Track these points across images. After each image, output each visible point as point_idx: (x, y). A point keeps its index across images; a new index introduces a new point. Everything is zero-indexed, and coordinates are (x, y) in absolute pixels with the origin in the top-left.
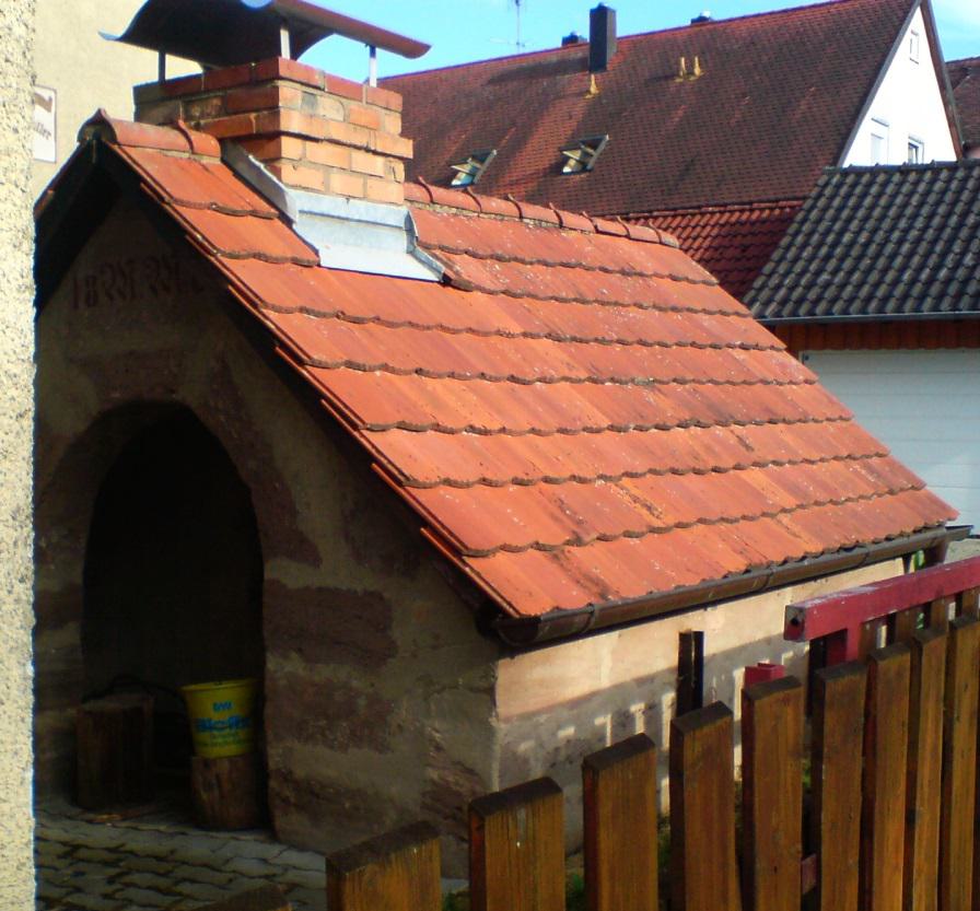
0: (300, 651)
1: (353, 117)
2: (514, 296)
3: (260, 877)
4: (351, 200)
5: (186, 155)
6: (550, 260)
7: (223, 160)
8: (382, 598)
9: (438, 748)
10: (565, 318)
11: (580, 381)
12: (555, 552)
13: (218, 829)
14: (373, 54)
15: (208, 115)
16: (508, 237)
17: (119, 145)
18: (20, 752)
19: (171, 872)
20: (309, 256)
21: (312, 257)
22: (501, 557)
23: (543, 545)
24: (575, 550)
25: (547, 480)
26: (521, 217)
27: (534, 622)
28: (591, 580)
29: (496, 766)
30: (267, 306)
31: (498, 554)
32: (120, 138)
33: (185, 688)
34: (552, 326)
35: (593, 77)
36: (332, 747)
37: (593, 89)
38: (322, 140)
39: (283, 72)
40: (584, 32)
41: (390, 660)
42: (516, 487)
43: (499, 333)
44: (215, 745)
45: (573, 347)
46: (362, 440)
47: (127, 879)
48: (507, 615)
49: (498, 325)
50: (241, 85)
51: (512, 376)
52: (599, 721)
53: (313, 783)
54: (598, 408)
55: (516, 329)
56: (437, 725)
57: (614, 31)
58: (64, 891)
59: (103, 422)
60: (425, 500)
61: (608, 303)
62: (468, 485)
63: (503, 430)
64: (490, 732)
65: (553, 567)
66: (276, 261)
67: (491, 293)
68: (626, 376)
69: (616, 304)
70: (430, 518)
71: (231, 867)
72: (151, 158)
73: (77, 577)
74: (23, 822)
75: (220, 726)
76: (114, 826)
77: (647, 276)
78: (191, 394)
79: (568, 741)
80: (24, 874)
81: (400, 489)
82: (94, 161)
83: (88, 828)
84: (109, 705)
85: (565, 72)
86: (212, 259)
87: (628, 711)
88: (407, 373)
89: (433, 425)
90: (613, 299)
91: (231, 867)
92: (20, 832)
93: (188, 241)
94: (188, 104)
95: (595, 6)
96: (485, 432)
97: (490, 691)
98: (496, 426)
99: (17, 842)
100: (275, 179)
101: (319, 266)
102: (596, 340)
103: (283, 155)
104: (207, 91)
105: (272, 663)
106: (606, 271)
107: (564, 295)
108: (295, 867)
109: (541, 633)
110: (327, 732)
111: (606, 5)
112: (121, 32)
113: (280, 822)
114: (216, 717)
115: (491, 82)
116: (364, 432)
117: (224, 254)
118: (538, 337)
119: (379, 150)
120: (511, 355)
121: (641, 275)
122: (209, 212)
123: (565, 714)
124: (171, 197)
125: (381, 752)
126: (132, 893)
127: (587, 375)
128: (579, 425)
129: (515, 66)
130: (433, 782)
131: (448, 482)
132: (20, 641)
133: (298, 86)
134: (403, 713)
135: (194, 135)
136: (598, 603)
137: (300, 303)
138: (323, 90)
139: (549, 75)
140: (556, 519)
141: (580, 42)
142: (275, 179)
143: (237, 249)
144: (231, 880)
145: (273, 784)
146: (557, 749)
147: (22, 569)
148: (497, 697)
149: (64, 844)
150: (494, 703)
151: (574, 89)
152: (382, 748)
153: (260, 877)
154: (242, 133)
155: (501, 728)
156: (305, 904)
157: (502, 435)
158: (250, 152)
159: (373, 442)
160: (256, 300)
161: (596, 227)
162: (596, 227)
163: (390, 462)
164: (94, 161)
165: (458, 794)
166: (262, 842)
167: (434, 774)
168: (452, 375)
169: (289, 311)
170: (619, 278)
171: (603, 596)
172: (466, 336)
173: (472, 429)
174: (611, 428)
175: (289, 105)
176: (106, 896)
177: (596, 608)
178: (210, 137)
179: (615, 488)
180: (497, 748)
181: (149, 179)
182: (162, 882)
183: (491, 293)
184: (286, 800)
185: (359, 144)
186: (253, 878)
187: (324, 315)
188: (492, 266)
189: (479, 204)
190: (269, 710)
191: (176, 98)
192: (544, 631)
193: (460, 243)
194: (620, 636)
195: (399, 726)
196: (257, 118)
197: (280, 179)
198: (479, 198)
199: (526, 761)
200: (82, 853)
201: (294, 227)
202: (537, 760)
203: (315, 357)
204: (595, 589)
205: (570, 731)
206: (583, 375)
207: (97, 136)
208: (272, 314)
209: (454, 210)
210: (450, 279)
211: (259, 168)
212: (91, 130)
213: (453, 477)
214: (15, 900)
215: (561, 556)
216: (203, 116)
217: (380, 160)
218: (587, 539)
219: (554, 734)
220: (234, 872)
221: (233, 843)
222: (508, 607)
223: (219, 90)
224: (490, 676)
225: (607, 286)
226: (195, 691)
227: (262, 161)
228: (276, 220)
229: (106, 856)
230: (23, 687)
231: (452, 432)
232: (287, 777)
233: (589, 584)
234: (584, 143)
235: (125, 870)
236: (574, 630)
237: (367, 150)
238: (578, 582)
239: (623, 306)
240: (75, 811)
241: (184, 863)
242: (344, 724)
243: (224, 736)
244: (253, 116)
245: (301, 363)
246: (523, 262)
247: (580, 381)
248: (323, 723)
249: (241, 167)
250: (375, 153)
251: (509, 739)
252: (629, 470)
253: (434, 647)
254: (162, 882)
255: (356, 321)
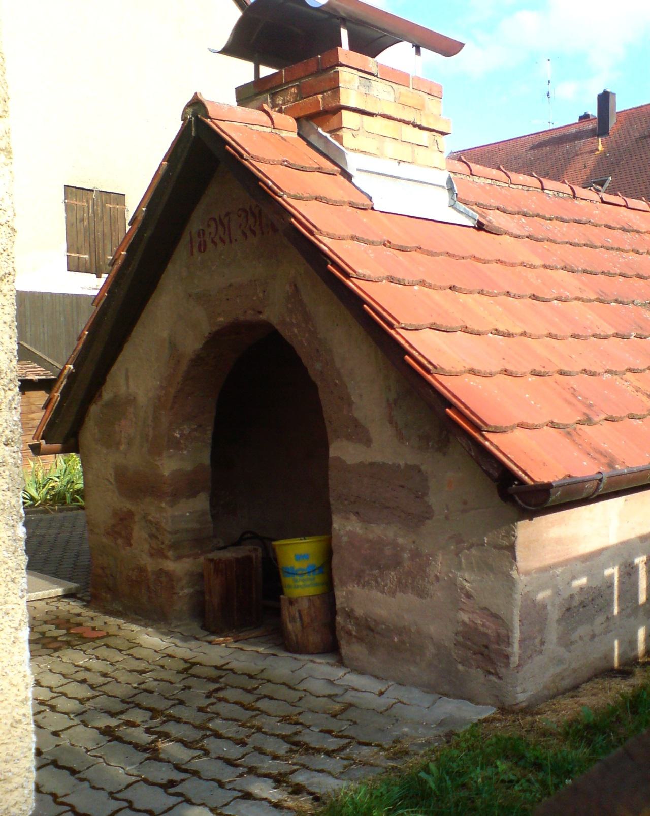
0: (357, 514)
1: (403, 99)
2: (537, 240)
3: (324, 696)
4: (402, 163)
5: (269, 130)
6: (565, 217)
7: (299, 134)
8: (420, 471)
9: (468, 596)
10: (580, 258)
11: (589, 301)
12: (568, 430)
13: (300, 653)
14: (418, 52)
15: (288, 101)
16: (532, 202)
17: (211, 119)
18: (12, 612)
19: (256, 689)
20: (362, 201)
21: (367, 202)
22: (518, 433)
23: (557, 424)
24: (586, 428)
25: (561, 373)
26: (543, 189)
27: (546, 489)
28: (601, 453)
29: (517, 612)
30: (321, 234)
31: (515, 430)
32: (211, 114)
33: (275, 543)
34: (567, 262)
35: (600, 139)
36: (383, 592)
37: (600, 148)
38: (377, 115)
39: (342, 59)
40: (594, 112)
41: (427, 521)
42: (534, 378)
43: (523, 264)
44: (297, 587)
45: (585, 277)
46: (397, 337)
47: (221, 694)
48: (522, 482)
49: (521, 258)
50: (311, 74)
51: (534, 295)
52: (607, 572)
53: (369, 620)
54: (605, 320)
55: (538, 262)
56: (467, 576)
57: (615, 106)
58: (171, 703)
59: (216, 340)
60: (451, 386)
61: (612, 249)
62: (491, 375)
63: (524, 334)
64: (511, 583)
65: (567, 441)
66: (335, 204)
67: (518, 237)
68: (627, 298)
69: (618, 249)
70: (454, 400)
71: (302, 686)
72: (237, 129)
73: (205, 458)
74: (17, 679)
75: (300, 572)
76: (226, 647)
77: (642, 233)
78: (272, 315)
79: (581, 589)
80: (19, 731)
81: (429, 377)
82: (193, 134)
83: (206, 648)
84: (228, 555)
85: (581, 138)
86: (280, 199)
87: (633, 563)
88: (441, 288)
89: (462, 327)
90: (616, 246)
91: (302, 686)
92: (15, 690)
93: (196, 130)
94: (274, 96)
95: (601, 92)
96: (509, 335)
97: (512, 548)
98: (518, 330)
99: (11, 699)
100: (337, 144)
101: (372, 209)
102: (603, 273)
103: (344, 125)
104: (287, 83)
105: (336, 524)
106: (610, 227)
107: (576, 241)
108: (353, 689)
109: (552, 498)
110: (379, 580)
111: (608, 90)
112: (221, 47)
113: (345, 650)
114: (297, 565)
115: (532, 148)
116: (399, 330)
117: (289, 196)
118: (556, 269)
119: (424, 125)
120: (534, 280)
121: (638, 232)
122: (281, 166)
123: (579, 566)
124: (249, 154)
125: (421, 597)
126: (221, 708)
127: (596, 297)
128: (590, 332)
129: (546, 137)
130: (464, 623)
131: (472, 372)
132: (7, 503)
133: (355, 71)
134: (439, 565)
135: (275, 115)
136: (606, 472)
137: (351, 232)
138: (376, 76)
139: (571, 141)
140: (570, 403)
141: (591, 118)
142: (337, 144)
143: (300, 193)
144: (300, 698)
145: (339, 619)
146: (572, 597)
147: (7, 432)
148: (517, 554)
149: (186, 661)
150: (515, 558)
151: (587, 149)
152: (422, 593)
153: (324, 696)
154: (313, 111)
155: (521, 580)
156: (355, 723)
157: (523, 338)
158: (319, 126)
159: (407, 338)
160: (314, 229)
161: (601, 198)
162: (601, 198)
163: (420, 354)
164: (193, 134)
165: (485, 634)
166: (332, 665)
167: (465, 617)
168: (481, 292)
169: (340, 238)
170: (619, 232)
171: (611, 465)
172: (494, 266)
173: (497, 332)
174: (616, 335)
175: (348, 86)
176: (200, 710)
177: (605, 475)
178: (288, 117)
179: (620, 380)
180: (518, 597)
181: (233, 143)
182: (247, 698)
183: (518, 237)
184: (349, 633)
185: (407, 119)
186: (318, 697)
187: (372, 243)
188: (519, 219)
189: (509, 177)
190: (335, 560)
191: (266, 91)
192: (554, 498)
193: (494, 203)
194: (626, 501)
195: (436, 576)
196: (323, 98)
197: (342, 144)
198: (509, 173)
199: (544, 607)
200: (196, 670)
201: (353, 180)
202: (553, 605)
203: (360, 271)
204: (604, 461)
205: (582, 581)
206: (593, 297)
207: (195, 114)
208: (326, 240)
209: (489, 181)
210: (483, 224)
211: (326, 137)
212: (190, 110)
213: (477, 367)
214: (8, 757)
215: (574, 433)
216: (284, 104)
217: (426, 133)
218: (596, 419)
219: (569, 584)
220: (305, 690)
221: (310, 665)
222: (523, 475)
223: (295, 81)
224: (511, 534)
225: (610, 237)
226: (281, 545)
227: (327, 132)
228: (338, 175)
229: (214, 673)
230: (12, 549)
231: (479, 334)
232: (350, 615)
233: (597, 456)
234: (594, 183)
235: (223, 685)
236: (584, 495)
237: (415, 125)
238: (589, 454)
239: (623, 251)
240: (201, 633)
241: (269, 681)
242: (392, 573)
243: (304, 580)
244: (320, 96)
245: (348, 276)
246: (544, 218)
247: (589, 301)
248: (376, 572)
249: (313, 139)
250: (421, 128)
251: (527, 589)
252: (632, 367)
253: (464, 511)
254: (247, 698)
255: (401, 249)
